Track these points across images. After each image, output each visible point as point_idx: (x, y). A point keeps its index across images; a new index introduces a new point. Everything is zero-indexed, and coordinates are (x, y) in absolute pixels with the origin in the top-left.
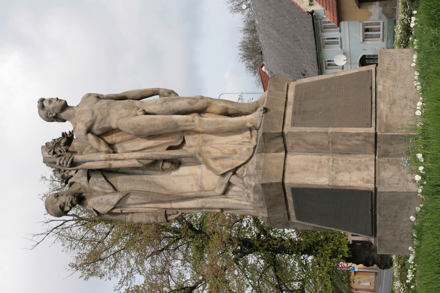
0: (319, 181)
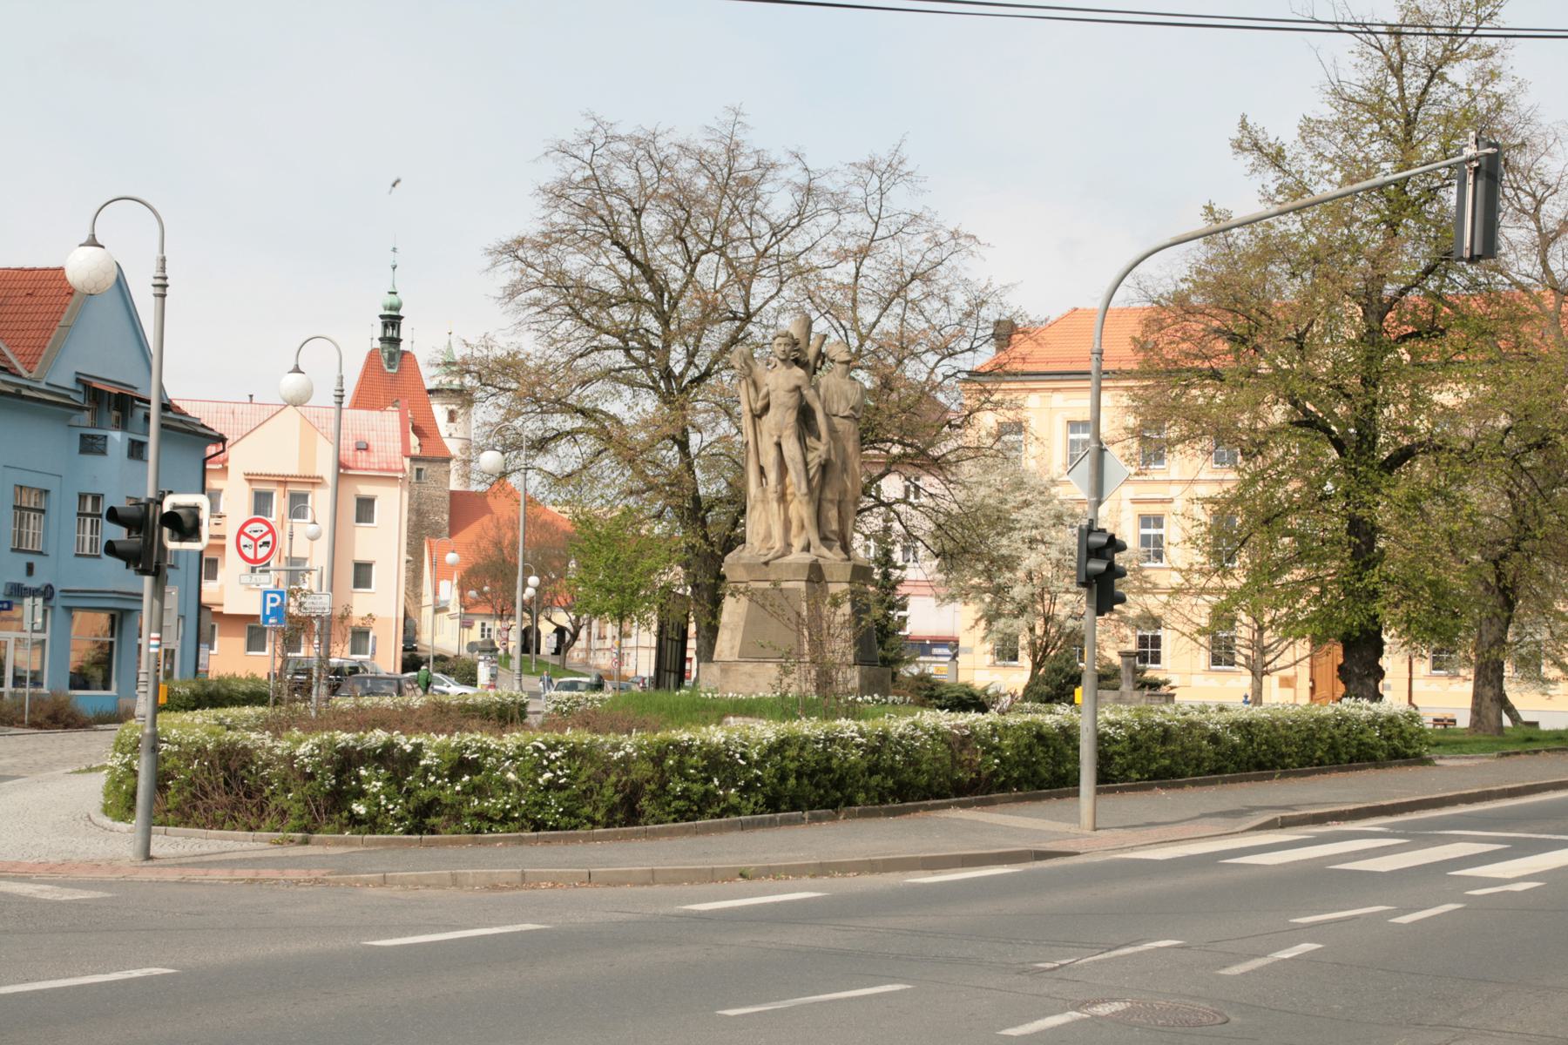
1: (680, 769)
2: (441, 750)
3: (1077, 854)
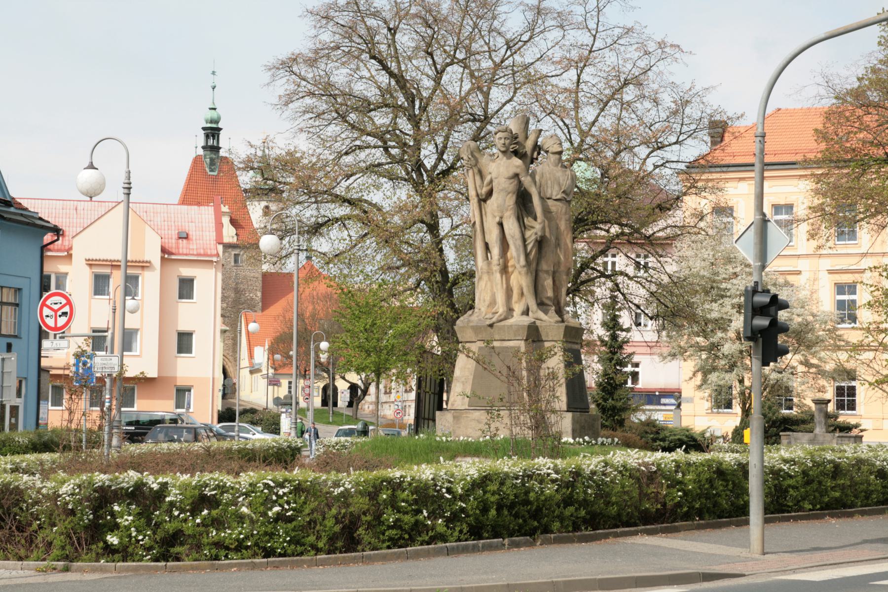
1: (393, 503)
2: (184, 487)
3: (743, 575)
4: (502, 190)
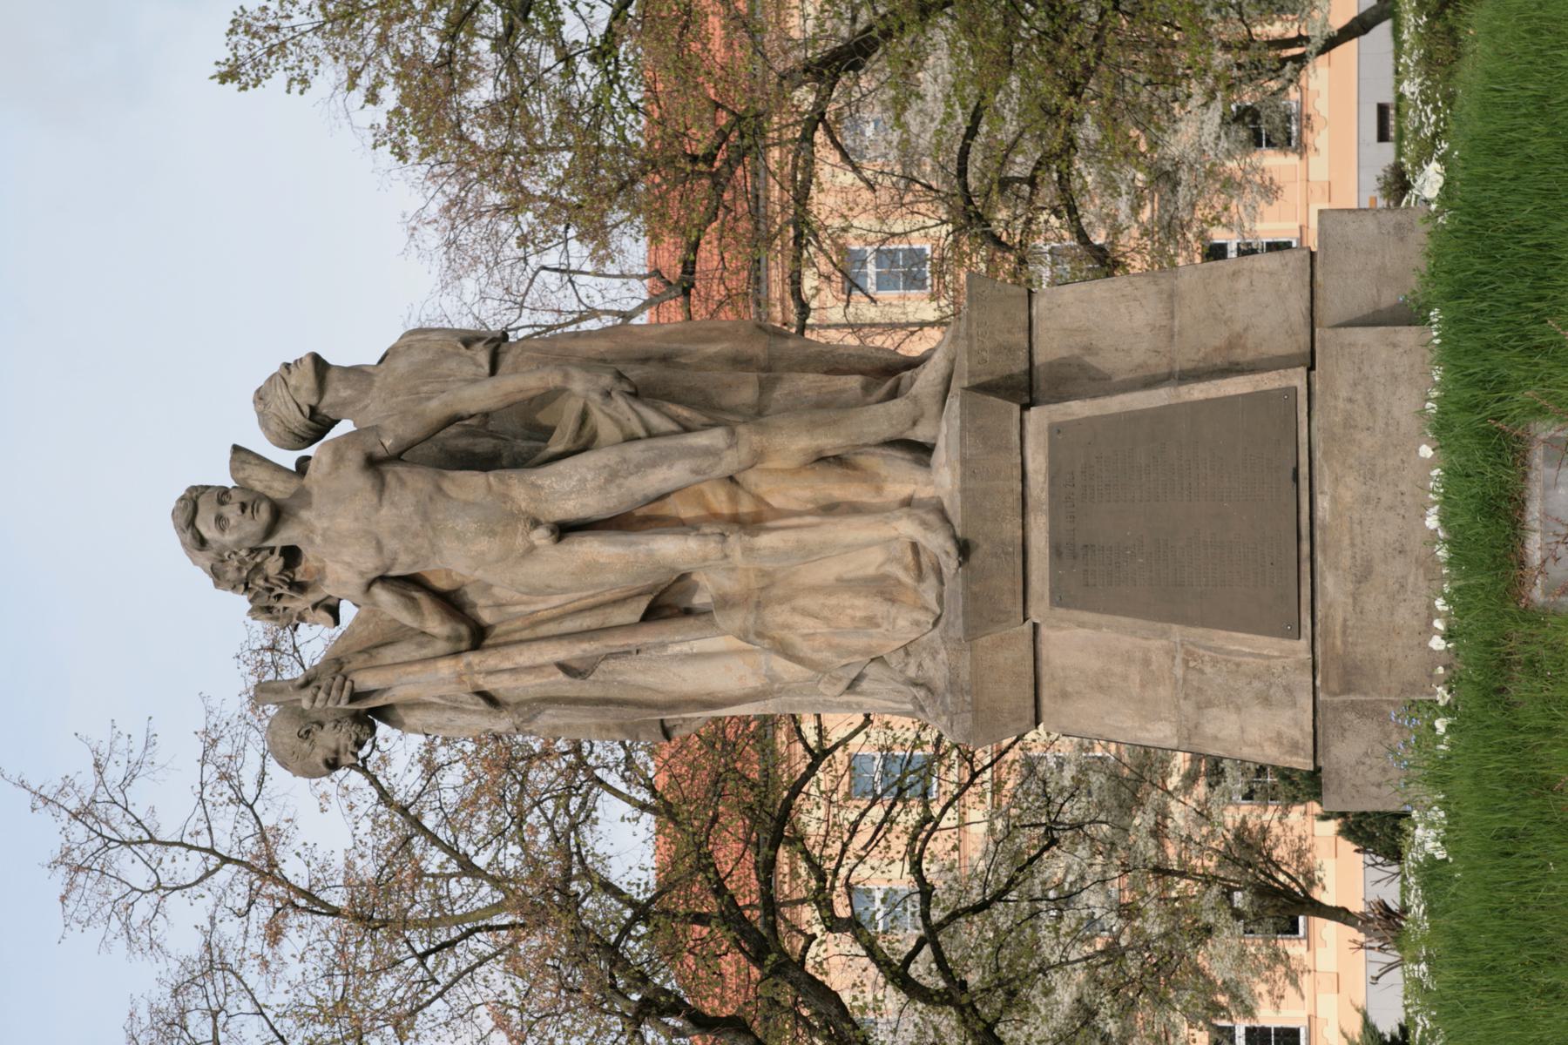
0: (1147, 735)
4: (426, 517)
